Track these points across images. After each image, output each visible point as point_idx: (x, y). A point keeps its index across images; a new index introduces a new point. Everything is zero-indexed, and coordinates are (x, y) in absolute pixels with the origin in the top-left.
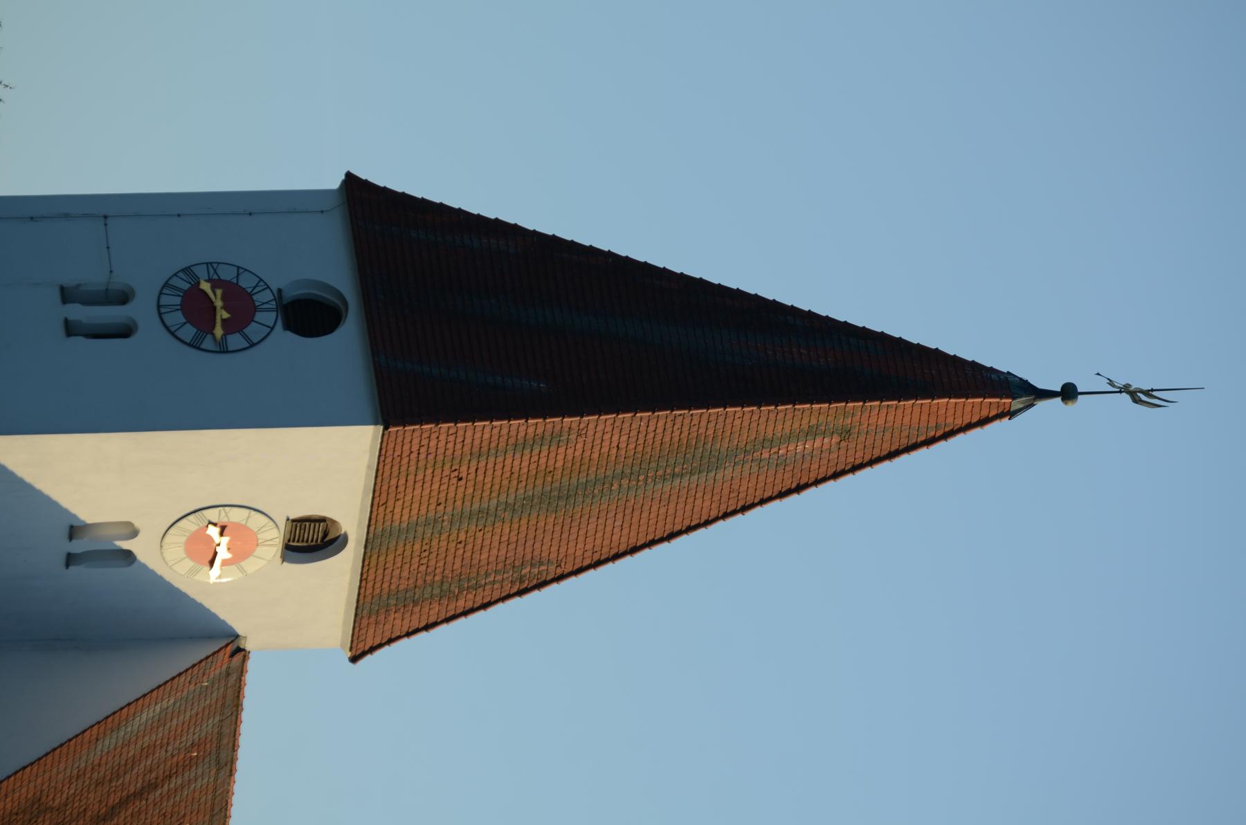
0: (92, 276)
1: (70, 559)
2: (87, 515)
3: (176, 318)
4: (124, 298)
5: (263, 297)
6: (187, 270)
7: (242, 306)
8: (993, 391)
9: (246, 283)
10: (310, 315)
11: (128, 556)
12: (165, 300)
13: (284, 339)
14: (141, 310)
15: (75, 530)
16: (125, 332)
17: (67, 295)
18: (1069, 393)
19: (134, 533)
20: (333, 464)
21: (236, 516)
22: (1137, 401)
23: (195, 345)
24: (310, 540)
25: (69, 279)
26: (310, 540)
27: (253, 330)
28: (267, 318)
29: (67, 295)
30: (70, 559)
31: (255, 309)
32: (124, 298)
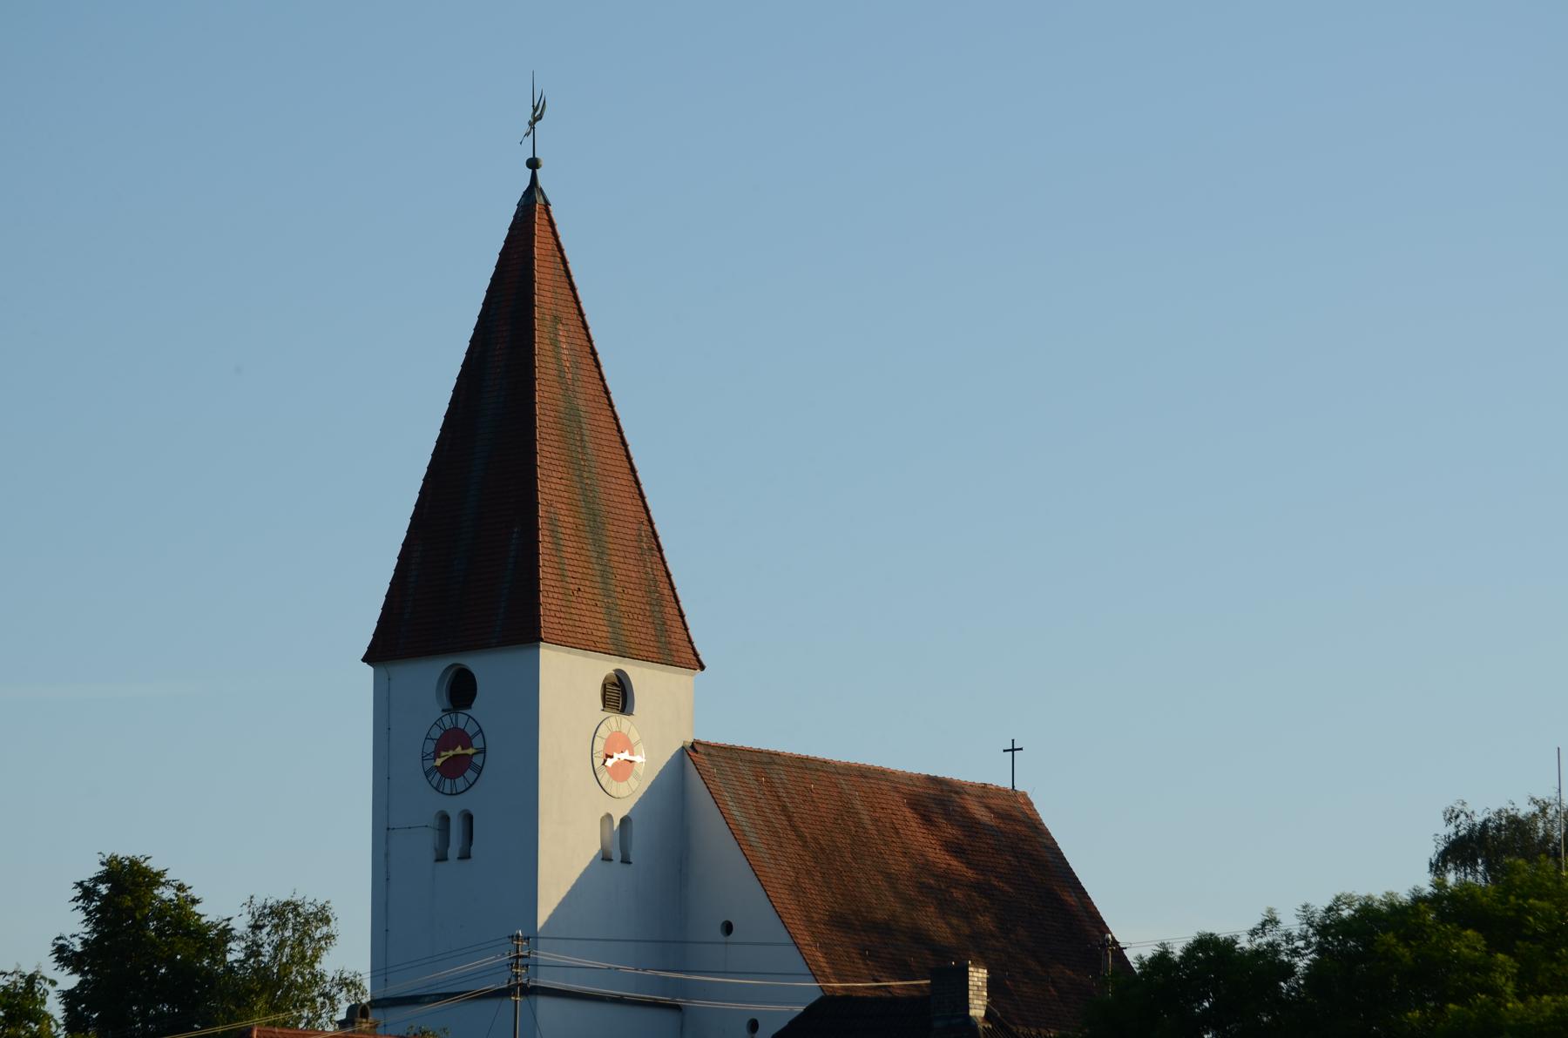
0: (429, 840)
1: (625, 860)
2: (595, 848)
3: (460, 783)
4: (445, 819)
5: (447, 722)
6: (427, 774)
7: (454, 737)
8: (530, 216)
9: (437, 733)
10: (461, 690)
11: (624, 821)
12: (447, 790)
13: (478, 707)
14: (454, 807)
15: (605, 857)
16: (468, 818)
17: (442, 857)
18: (533, 164)
19: (609, 816)
20: (566, 678)
21: (599, 746)
22: (540, 117)
23: (479, 771)
24: (618, 695)
25: (430, 855)
26: (618, 695)
27: (471, 730)
28: (462, 720)
29: (442, 857)
30: (625, 860)
31: (456, 728)
32: (445, 819)
